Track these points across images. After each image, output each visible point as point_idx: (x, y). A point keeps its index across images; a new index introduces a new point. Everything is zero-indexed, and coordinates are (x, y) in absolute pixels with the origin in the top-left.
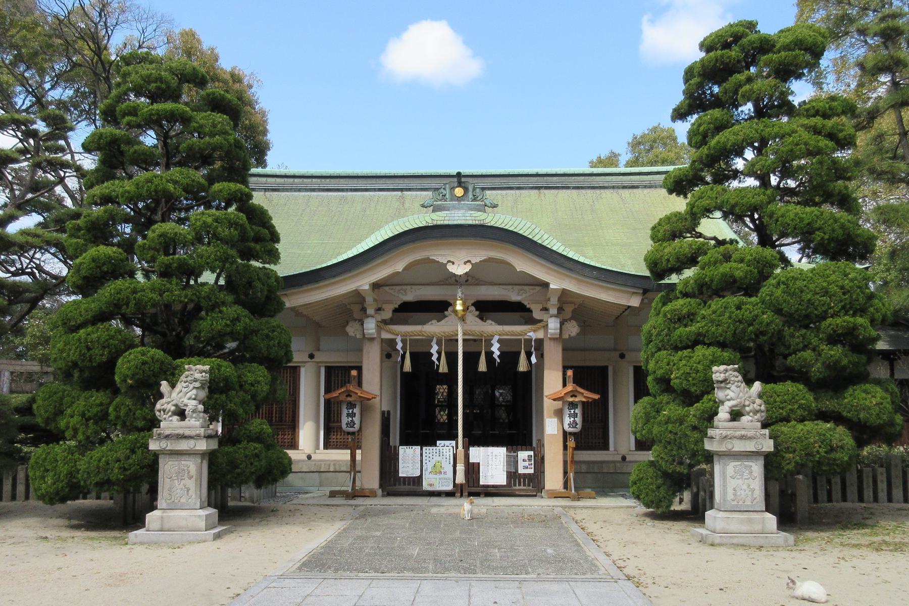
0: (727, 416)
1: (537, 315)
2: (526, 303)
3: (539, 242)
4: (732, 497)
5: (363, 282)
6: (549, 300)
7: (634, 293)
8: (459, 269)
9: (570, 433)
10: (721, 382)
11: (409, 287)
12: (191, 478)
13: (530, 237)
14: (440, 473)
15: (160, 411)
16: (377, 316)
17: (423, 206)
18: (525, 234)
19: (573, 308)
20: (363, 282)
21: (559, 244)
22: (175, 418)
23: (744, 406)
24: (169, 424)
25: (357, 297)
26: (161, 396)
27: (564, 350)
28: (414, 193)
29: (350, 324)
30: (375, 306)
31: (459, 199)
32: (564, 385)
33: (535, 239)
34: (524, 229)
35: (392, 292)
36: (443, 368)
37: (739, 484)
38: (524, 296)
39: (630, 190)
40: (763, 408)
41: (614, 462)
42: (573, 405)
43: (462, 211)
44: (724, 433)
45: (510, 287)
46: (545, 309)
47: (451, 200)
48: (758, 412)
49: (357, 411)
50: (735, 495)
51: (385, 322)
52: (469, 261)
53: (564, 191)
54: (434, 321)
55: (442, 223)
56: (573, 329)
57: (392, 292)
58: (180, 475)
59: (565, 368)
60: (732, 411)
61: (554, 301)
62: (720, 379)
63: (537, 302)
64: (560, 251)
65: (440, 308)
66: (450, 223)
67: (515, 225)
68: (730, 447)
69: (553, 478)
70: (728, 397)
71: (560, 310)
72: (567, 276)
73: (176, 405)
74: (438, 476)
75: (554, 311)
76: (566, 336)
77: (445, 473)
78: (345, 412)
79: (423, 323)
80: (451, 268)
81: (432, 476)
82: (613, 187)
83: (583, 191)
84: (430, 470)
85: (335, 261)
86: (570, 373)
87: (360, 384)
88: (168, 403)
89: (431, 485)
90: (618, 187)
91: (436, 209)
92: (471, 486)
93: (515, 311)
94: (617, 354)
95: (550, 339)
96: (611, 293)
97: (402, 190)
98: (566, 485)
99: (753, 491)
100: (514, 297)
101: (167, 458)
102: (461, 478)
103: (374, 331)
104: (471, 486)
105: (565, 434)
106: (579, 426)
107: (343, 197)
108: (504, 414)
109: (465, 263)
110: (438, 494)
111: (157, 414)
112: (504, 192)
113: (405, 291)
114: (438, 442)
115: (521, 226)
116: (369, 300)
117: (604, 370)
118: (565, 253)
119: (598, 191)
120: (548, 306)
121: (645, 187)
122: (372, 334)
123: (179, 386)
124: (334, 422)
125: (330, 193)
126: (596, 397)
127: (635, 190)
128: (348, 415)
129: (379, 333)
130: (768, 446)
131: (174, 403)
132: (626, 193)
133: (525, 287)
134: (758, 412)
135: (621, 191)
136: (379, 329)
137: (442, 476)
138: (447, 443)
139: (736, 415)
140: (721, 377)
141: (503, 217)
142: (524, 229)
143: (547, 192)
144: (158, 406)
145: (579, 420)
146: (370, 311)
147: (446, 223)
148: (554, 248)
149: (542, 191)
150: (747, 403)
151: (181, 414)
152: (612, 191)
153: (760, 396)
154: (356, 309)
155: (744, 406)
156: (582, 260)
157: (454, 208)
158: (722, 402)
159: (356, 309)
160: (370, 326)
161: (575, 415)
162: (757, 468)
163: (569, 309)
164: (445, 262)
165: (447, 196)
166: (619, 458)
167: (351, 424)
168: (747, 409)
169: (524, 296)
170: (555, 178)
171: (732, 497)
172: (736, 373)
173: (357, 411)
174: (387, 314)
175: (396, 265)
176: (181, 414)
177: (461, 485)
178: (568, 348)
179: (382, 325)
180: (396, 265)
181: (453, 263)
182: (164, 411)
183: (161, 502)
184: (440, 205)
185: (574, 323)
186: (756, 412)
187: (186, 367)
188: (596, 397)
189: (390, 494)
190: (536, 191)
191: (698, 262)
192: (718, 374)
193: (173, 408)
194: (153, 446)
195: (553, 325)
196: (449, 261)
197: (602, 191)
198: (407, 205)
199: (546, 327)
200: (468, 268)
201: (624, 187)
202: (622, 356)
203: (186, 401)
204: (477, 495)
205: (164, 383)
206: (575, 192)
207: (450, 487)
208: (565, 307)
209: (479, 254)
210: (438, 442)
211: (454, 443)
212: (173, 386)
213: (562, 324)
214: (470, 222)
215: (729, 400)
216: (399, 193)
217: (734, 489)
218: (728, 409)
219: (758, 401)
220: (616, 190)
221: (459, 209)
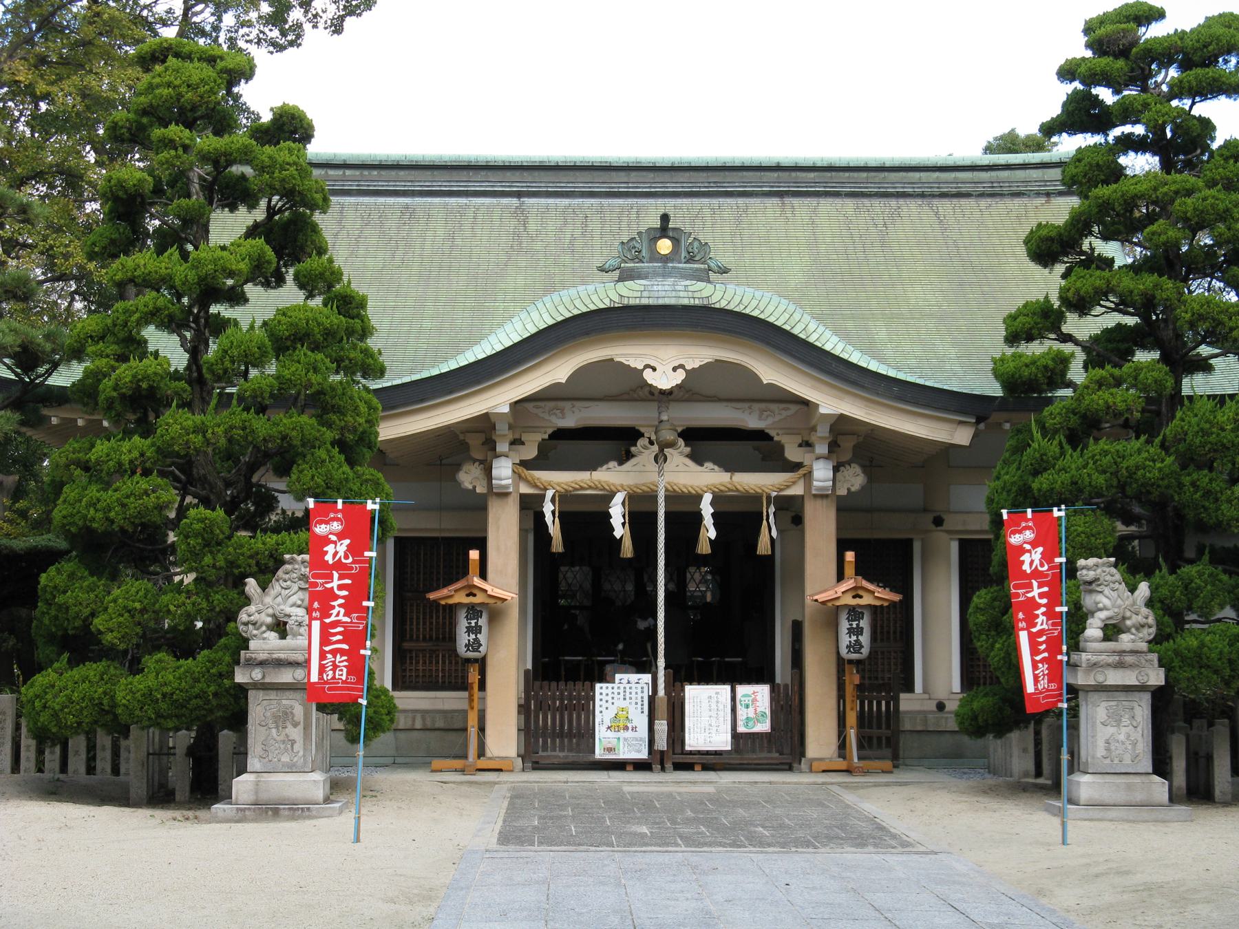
0: (1099, 633)
1: (793, 453)
2: (772, 433)
3: (802, 336)
4: (1104, 753)
5: (496, 401)
6: (814, 429)
7: (961, 423)
8: (664, 379)
9: (850, 662)
10: (1090, 583)
11: (567, 405)
12: (295, 725)
13: (787, 327)
14: (626, 728)
15: (246, 624)
16: (511, 454)
17: (602, 269)
18: (778, 323)
19: (852, 443)
20: (496, 401)
21: (835, 339)
22: (273, 635)
23: (1124, 618)
24: (264, 644)
25: (485, 423)
26: (248, 601)
27: (839, 510)
28: (543, 201)
29: (466, 467)
30: (511, 437)
31: (665, 259)
32: (840, 577)
33: (795, 331)
34: (776, 314)
35: (535, 411)
36: (627, 550)
37: (1116, 733)
38: (770, 421)
39: (955, 201)
40: (1151, 620)
41: (924, 713)
42: (855, 613)
43: (670, 281)
44: (1094, 658)
45: (746, 405)
46: (807, 444)
47: (651, 260)
48: (1143, 626)
49: (483, 621)
50: (1108, 750)
51: (525, 464)
52: (682, 366)
53: (830, 200)
54: (613, 464)
55: (637, 302)
56: (854, 479)
57: (535, 411)
58: (283, 718)
59: (843, 545)
60: (1106, 625)
61: (823, 431)
62: (1088, 579)
63: (790, 431)
64: (837, 352)
65: (620, 442)
66: (652, 302)
67: (762, 307)
68: (1100, 679)
69: (820, 736)
70: (1100, 605)
71: (833, 446)
72: (848, 393)
73: (274, 616)
74: (623, 734)
75: (822, 449)
76: (842, 492)
77: (634, 729)
78: (462, 624)
79: (592, 466)
80: (649, 376)
81: (610, 734)
82: (922, 195)
83: (866, 201)
84: (607, 723)
85: (453, 365)
86: (850, 556)
87: (483, 575)
88: (259, 612)
89: (610, 750)
90: (933, 196)
91: (626, 276)
92: (672, 755)
93: (755, 448)
94: (930, 517)
95: (815, 496)
96: (921, 422)
97: (519, 195)
98: (842, 746)
99: (1134, 744)
100: (752, 421)
101: (261, 694)
102: (662, 743)
103: (510, 481)
104: (672, 755)
105: (841, 663)
106: (865, 651)
107: (407, 207)
108: (729, 624)
109: (675, 369)
110: (620, 766)
111: (241, 628)
112: (715, 201)
113: (562, 410)
114: (618, 676)
115: (771, 308)
116: (502, 428)
117: (905, 546)
118: (845, 356)
119: (893, 202)
120: (813, 439)
121: (982, 195)
122: (507, 487)
123: (275, 588)
124: (411, 639)
125: (381, 200)
126: (896, 598)
127: (964, 201)
128: (470, 630)
129: (517, 486)
130: (1156, 678)
131: (270, 611)
132: (945, 206)
133: (773, 406)
134: (1143, 626)
135: (936, 202)
136: (518, 477)
137: (629, 734)
138: (634, 677)
139: (1112, 631)
140: (1091, 575)
141: (740, 290)
142: (776, 314)
143: (796, 201)
144: (243, 617)
145: (865, 639)
146: (502, 447)
147: (645, 302)
148: (828, 347)
149: (787, 200)
150: (1128, 614)
151: (280, 627)
152: (919, 201)
153: (1150, 603)
154: (475, 441)
155: (1124, 618)
156: (873, 366)
157: (655, 274)
158: (1092, 613)
159: (475, 441)
160: (503, 471)
161: (859, 631)
162: (1142, 709)
163: (848, 444)
164: (641, 367)
165: (644, 253)
166: (932, 706)
167: (475, 645)
168: (1128, 623)
169: (770, 421)
170: (812, 175)
171: (1104, 753)
172: (1113, 570)
173: (483, 621)
174: (530, 452)
175: (557, 371)
176: (280, 627)
177: (662, 752)
178: (846, 508)
179: (521, 469)
180: (557, 371)
181: (654, 369)
182: (254, 624)
183: (253, 763)
184: (632, 269)
185: (856, 469)
186: (1140, 627)
187: (287, 556)
188: (896, 598)
189: (537, 766)
190: (776, 200)
191: (1168, 173)
192: (1084, 572)
193: (269, 620)
194: (240, 677)
195: (822, 473)
196: (647, 366)
197: (901, 201)
198: (532, 226)
199: (808, 476)
200: (680, 377)
201: (943, 195)
202: (938, 522)
203: (288, 610)
204: (688, 767)
205: (251, 582)
206: (850, 203)
207: (643, 755)
208: (841, 440)
209: (697, 355)
210: (618, 676)
211: (647, 678)
212: (264, 587)
213: (836, 469)
214: (685, 302)
215: (1101, 610)
216: (514, 201)
217: (1107, 742)
218: (1101, 624)
219: (1145, 611)
220: (926, 201)
221: (665, 275)
